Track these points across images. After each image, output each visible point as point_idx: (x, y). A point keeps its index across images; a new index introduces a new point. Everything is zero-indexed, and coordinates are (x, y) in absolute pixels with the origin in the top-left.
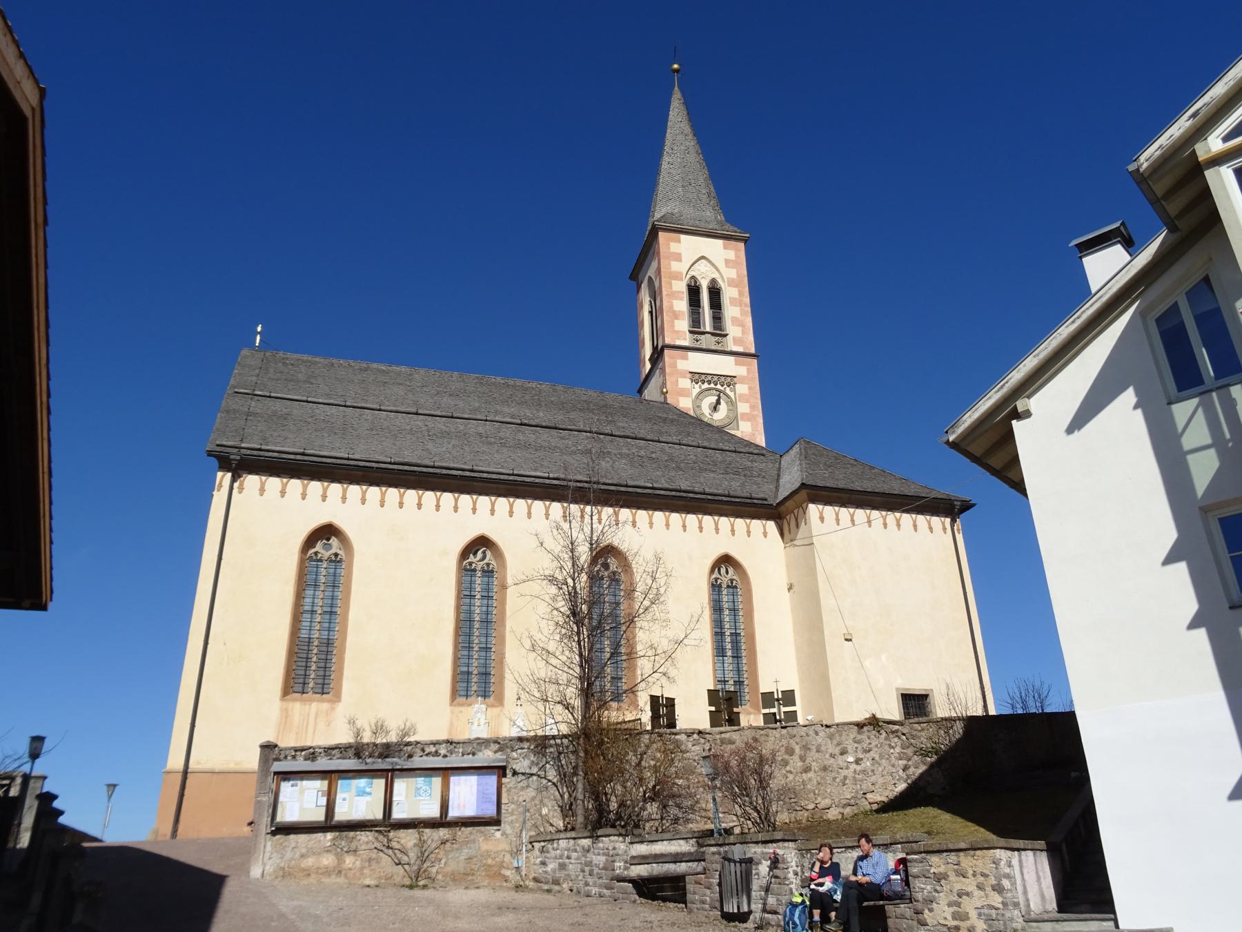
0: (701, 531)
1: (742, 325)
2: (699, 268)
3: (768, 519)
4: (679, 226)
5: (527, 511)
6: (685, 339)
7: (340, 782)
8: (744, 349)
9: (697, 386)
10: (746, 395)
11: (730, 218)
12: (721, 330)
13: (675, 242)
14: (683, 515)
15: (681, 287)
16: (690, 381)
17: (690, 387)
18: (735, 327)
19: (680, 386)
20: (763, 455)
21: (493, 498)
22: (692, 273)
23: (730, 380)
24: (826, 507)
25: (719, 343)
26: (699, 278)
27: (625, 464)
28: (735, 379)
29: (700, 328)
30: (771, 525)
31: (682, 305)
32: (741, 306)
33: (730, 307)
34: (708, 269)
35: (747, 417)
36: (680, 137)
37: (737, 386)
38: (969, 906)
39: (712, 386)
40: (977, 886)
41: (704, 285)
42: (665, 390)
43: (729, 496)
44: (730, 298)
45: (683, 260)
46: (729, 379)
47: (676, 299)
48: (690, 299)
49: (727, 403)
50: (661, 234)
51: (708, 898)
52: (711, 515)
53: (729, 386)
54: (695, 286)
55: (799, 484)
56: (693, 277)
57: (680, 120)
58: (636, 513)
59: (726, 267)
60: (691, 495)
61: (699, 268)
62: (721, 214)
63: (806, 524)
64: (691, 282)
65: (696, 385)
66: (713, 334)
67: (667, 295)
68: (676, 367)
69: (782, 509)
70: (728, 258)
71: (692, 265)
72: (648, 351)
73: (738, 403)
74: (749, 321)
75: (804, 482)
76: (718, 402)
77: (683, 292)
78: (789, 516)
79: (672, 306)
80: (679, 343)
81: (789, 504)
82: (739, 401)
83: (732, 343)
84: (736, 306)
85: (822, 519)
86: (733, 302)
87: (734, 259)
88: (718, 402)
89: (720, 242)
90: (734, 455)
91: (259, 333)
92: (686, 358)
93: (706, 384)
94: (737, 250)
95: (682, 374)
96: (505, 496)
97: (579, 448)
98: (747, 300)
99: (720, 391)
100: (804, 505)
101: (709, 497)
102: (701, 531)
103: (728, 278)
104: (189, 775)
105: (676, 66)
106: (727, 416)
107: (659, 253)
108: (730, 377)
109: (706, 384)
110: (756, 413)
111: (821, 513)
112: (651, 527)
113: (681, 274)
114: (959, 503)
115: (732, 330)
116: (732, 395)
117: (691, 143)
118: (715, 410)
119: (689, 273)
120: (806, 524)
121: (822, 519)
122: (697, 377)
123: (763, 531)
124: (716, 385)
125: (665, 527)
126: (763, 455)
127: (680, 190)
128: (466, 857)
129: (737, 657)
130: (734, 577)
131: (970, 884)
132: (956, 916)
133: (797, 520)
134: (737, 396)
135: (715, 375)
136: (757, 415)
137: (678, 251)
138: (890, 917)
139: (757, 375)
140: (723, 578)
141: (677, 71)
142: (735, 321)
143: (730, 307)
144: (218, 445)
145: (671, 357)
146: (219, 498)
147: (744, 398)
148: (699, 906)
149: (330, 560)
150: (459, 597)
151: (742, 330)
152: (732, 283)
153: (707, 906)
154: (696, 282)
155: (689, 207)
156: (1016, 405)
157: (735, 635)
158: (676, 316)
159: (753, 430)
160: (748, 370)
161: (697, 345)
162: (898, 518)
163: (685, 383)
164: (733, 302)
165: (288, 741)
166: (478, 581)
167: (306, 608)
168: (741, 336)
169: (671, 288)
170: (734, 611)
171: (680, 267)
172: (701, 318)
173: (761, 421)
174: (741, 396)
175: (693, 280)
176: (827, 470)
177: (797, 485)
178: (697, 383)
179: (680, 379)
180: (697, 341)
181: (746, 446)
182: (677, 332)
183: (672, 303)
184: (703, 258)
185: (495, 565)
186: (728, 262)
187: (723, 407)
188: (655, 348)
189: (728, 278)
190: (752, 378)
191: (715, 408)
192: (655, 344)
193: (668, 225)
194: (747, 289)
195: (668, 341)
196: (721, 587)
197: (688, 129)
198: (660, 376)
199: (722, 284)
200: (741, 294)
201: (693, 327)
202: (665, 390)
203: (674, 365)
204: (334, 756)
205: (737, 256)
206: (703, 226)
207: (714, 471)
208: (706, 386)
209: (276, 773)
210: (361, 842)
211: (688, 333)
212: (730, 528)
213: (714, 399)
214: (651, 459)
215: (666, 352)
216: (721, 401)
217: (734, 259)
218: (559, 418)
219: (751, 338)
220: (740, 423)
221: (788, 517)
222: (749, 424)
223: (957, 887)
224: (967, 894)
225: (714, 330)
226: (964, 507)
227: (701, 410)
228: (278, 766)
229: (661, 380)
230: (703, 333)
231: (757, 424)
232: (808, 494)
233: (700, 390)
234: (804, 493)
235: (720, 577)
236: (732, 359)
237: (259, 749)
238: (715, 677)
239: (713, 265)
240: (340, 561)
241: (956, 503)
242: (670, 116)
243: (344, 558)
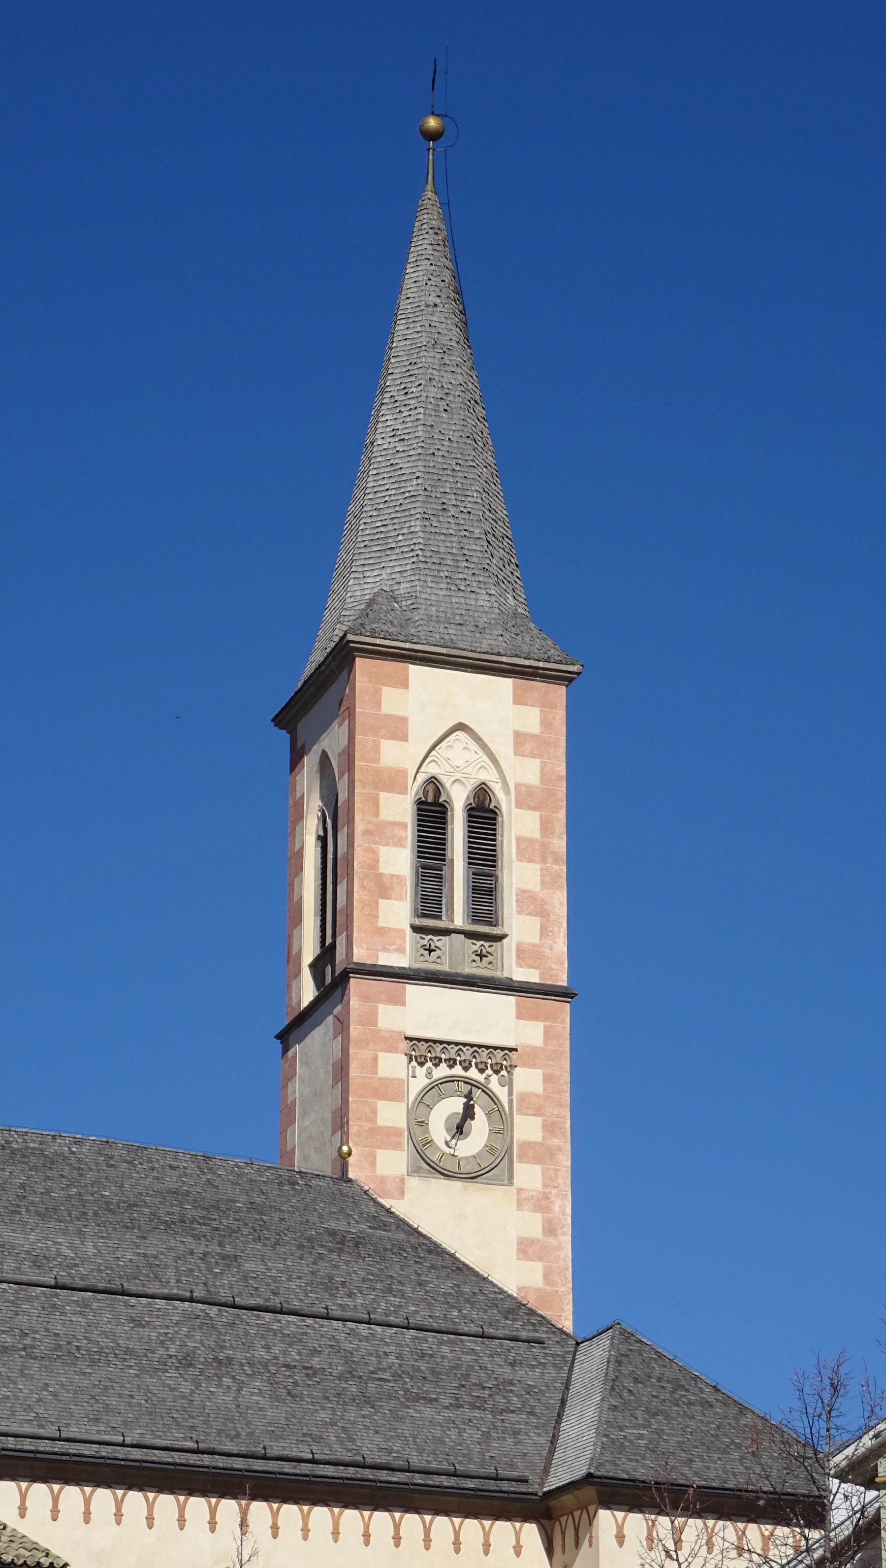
0: (397, 1545)
1: (542, 911)
2: (449, 753)
3: (526, 1519)
4: (407, 645)
5: (83, 1509)
6: (401, 950)
8: (542, 976)
9: (421, 1071)
10: (537, 1096)
12: (490, 924)
13: (395, 686)
14: (366, 1514)
16: (405, 1059)
17: (402, 1075)
18: (527, 918)
19: (381, 1122)
20: (540, 1342)
21: (24, 1485)
22: (430, 769)
24: (631, 1515)
25: (481, 956)
26: (446, 781)
27: (261, 1393)
28: (513, 1055)
29: (439, 918)
30: (531, 1532)
32: (543, 860)
33: (516, 864)
35: (533, 1153)
36: (430, 358)
37: (517, 1071)
39: (458, 1070)
42: (345, 1149)
43: (455, 1474)
44: (518, 839)
45: (410, 738)
46: (499, 1054)
47: (387, 845)
48: (421, 840)
49: (489, 1114)
50: (361, 664)
52: (419, 1513)
53: (497, 1072)
54: (436, 803)
57: (433, 299)
58: (278, 1509)
59: (516, 754)
61: (449, 753)
63: (590, 1545)
64: (426, 793)
65: (418, 1068)
66: (471, 935)
67: (366, 832)
68: (375, 1023)
69: (554, 1503)
70: (521, 729)
71: (433, 748)
73: (517, 1118)
75: (592, 1471)
76: (468, 1113)
77: (404, 825)
78: (566, 1517)
79: (374, 864)
80: (387, 959)
81: (567, 1499)
82: (520, 1112)
83: (514, 958)
84: (531, 861)
85: (620, 1539)
86: (526, 849)
87: (536, 730)
88: (468, 1113)
89: (506, 684)
92: (400, 1001)
93: (443, 1065)
94: (546, 704)
95: (388, 1043)
96: (44, 1480)
97: (172, 1351)
98: (560, 844)
99: (472, 1084)
100: (591, 1508)
102: (397, 1545)
105: (432, 123)
106: (489, 1149)
107: (351, 714)
108: (503, 1049)
109: (443, 1065)
110: (556, 1141)
111: (620, 1528)
112: (305, 1538)
113: (404, 773)
116: (502, 1093)
118: (461, 1133)
119: (422, 769)
120: (590, 1545)
121: (620, 1539)
123: (514, 1543)
124: (466, 1069)
125: (331, 1536)
126: (540, 1342)
133: (577, 1530)
134: (514, 1097)
135: (465, 1045)
136: (559, 1149)
137: (401, 713)
139: (567, 1043)
141: (433, 136)
142: (527, 901)
143: (516, 864)
145: (366, 998)
151: (542, 927)
154: (438, 793)
155: (437, 579)
156: (877, 1465)
159: (545, 1186)
160: (548, 1034)
161: (429, 964)
162: (767, 1533)
168: (536, 940)
169: (377, 814)
172: (445, 890)
173: (565, 1161)
174: (524, 1097)
175: (431, 788)
177: (581, 1472)
178: (421, 1064)
179: (381, 1055)
180: (430, 951)
182: (383, 931)
183: (375, 853)
184: (461, 727)
187: (480, 1125)
189: (517, 786)
190: (555, 1051)
191: (460, 1130)
192: (329, 941)
193: (378, 641)
194: (562, 814)
195: (360, 955)
197: (451, 334)
198: (335, 1037)
199: (503, 800)
200: (546, 827)
201: (424, 916)
202: (345, 1149)
203: (371, 1019)
205: (545, 723)
207: (431, 1400)
208: (443, 1071)
211: (409, 930)
212: (452, 1538)
213: (456, 1104)
214: (311, 1372)
215: (355, 984)
216: (477, 1109)
217: (536, 730)
219: (561, 945)
220: (516, 1165)
221: (563, 1519)
222: (537, 1169)
225: (475, 922)
227: (427, 1131)
230: (446, 932)
231: (556, 1170)
233: (428, 1081)
234: (590, 1492)
236: (508, 1002)
239: (484, 747)
242: (408, 282)
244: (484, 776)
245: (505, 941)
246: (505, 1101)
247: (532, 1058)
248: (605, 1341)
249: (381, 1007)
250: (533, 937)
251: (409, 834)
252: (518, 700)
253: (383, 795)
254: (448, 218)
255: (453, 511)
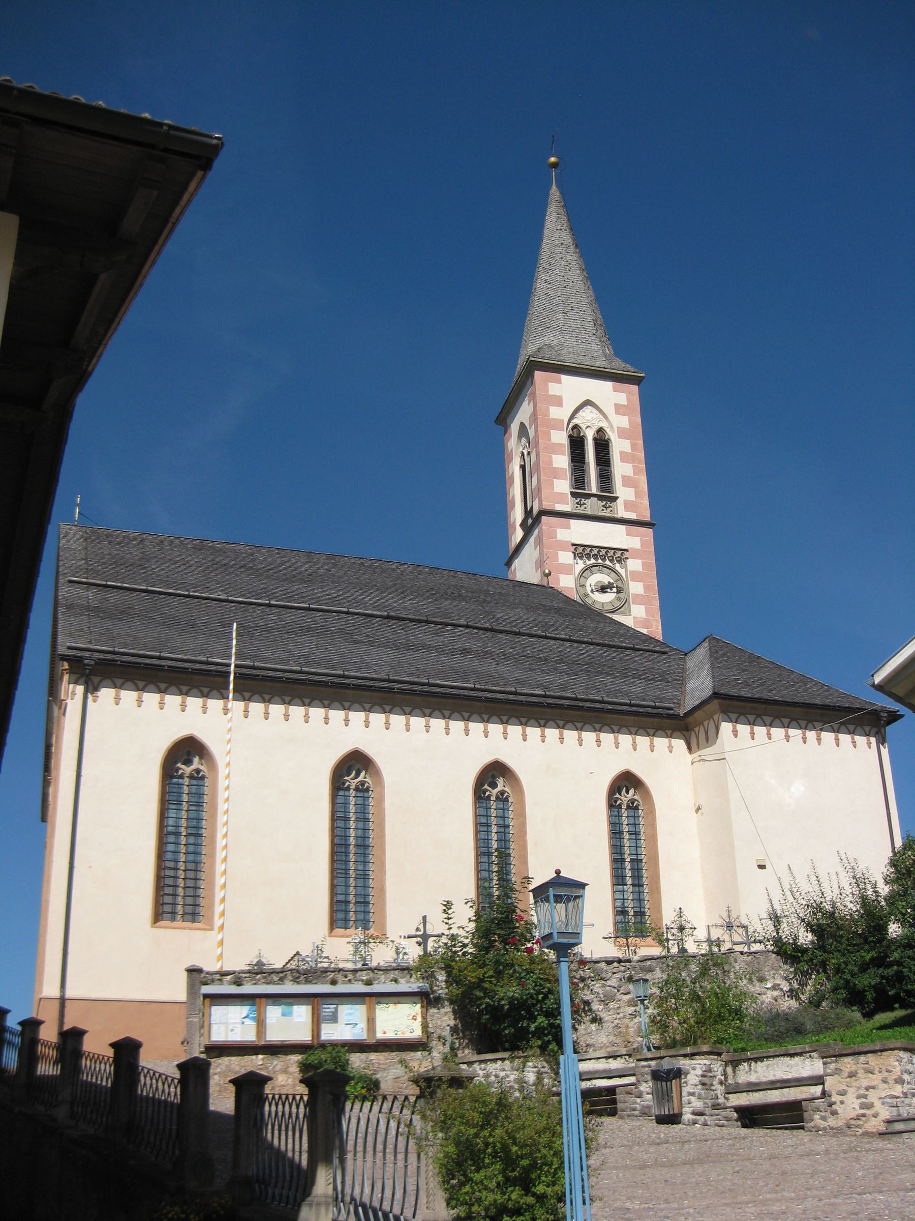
7: (269, 1008)
11: (619, 352)
15: (561, 438)
16: (572, 555)
22: (575, 421)
23: (619, 555)
29: (584, 489)
31: (562, 461)
34: (593, 415)
35: (639, 600)
38: (873, 1097)
40: (882, 1081)
41: (590, 435)
44: (621, 453)
50: (538, 374)
51: (638, 1106)
55: (710, 693)
56: (576, 427)
59: (616, 413)
60: (588, 704)
62: (610, 347)
66: (600, 498)
69: (690, 719)
72: (518, 515)
74: (643, 480)
80: (559, 507)
81: (698, 714)
82: (632, 580)
90: (632, 653)
91: (78, 505)
95: (562, 546)
98: (642, 455)
101: (609, 707)
103: (618, 428)
104: (68, 1003)
105: (553, 159)
107: (534, 395)
114: (885, 715)
115: (623, 492)
116: (622, 572)
117: (572, 257)
122: (581, 551)
124: (604, 560)
127: (561, 316)
128: (394, 1077)
129: (638, 884)
130: (636, 797)
131: (876, 1079)
132: (863, 1106)
133: (706, 733)
138: (806, 1111)
140: (622, 798)
141: (555, 165)
142: (627, 481)
144: (69, 648)
146: (73, 706)
147: (636, 576)
148: (629, 1113)
149: (191, 777)
150: (334, 818)
152: (622, 433)
153: (637, 1113)
157: (636, 861)
158: (556, 473)
161: (580, 510)
163: (566, 557)
164: (625, 457)
165: (210, 965)
166: (352, 800)
167: (170, 829)
170: (635, 834)
171: (561, 413)
174: (633, 572)
176: (740, 675)
177: (708, 693)
180: (581, 505)
181: (644, 642)
184: (587, 403)
185: (370, 782)
186: (619, 409)
188: (528, 513)
189: (618, 428)
196: (621, 808)
199: (613, 436)
200: (633, 446)
204: (259, 980)
206: (587, 362)
208: (593, 561)
209: (206, 996)
210: (292, 1061)
211: (570, 496)
217: (625, 403)
218: (427, 608)
219: (646, 502)
220: (632, 605)
221: (696, 729)
223: (865, 1083)
224: (873, 1088)
225: (602, 492)
226: (892, 718)
228: (206, 989)
229: (536, 554)
232: (720, 705)
235: (619, 797)
236: (622, 528)
237: (185, 974)
238: (615, 907)
240: (203, 778)
241: (882, 714)
243: (207, 774)
244: (601, 425)
245: (618, 501)
246: (623, 574)
247: (637, 554)
248: (706, 644)
249: (558, 530)
250: (632, 498)
251: (567, 449)
252: (615, 390)
253: (552, 431)
254: (562, 193)
255: (578, 310)
